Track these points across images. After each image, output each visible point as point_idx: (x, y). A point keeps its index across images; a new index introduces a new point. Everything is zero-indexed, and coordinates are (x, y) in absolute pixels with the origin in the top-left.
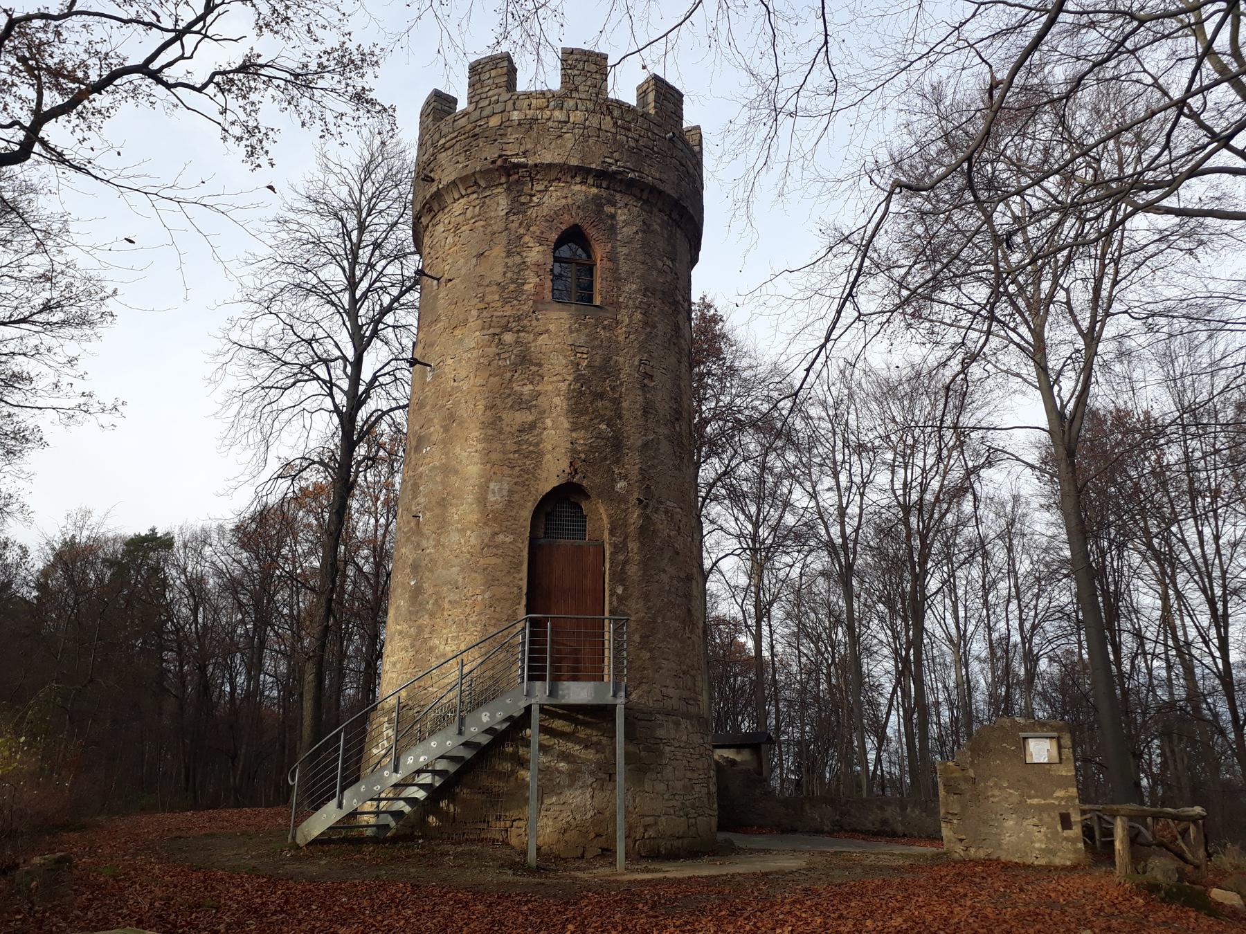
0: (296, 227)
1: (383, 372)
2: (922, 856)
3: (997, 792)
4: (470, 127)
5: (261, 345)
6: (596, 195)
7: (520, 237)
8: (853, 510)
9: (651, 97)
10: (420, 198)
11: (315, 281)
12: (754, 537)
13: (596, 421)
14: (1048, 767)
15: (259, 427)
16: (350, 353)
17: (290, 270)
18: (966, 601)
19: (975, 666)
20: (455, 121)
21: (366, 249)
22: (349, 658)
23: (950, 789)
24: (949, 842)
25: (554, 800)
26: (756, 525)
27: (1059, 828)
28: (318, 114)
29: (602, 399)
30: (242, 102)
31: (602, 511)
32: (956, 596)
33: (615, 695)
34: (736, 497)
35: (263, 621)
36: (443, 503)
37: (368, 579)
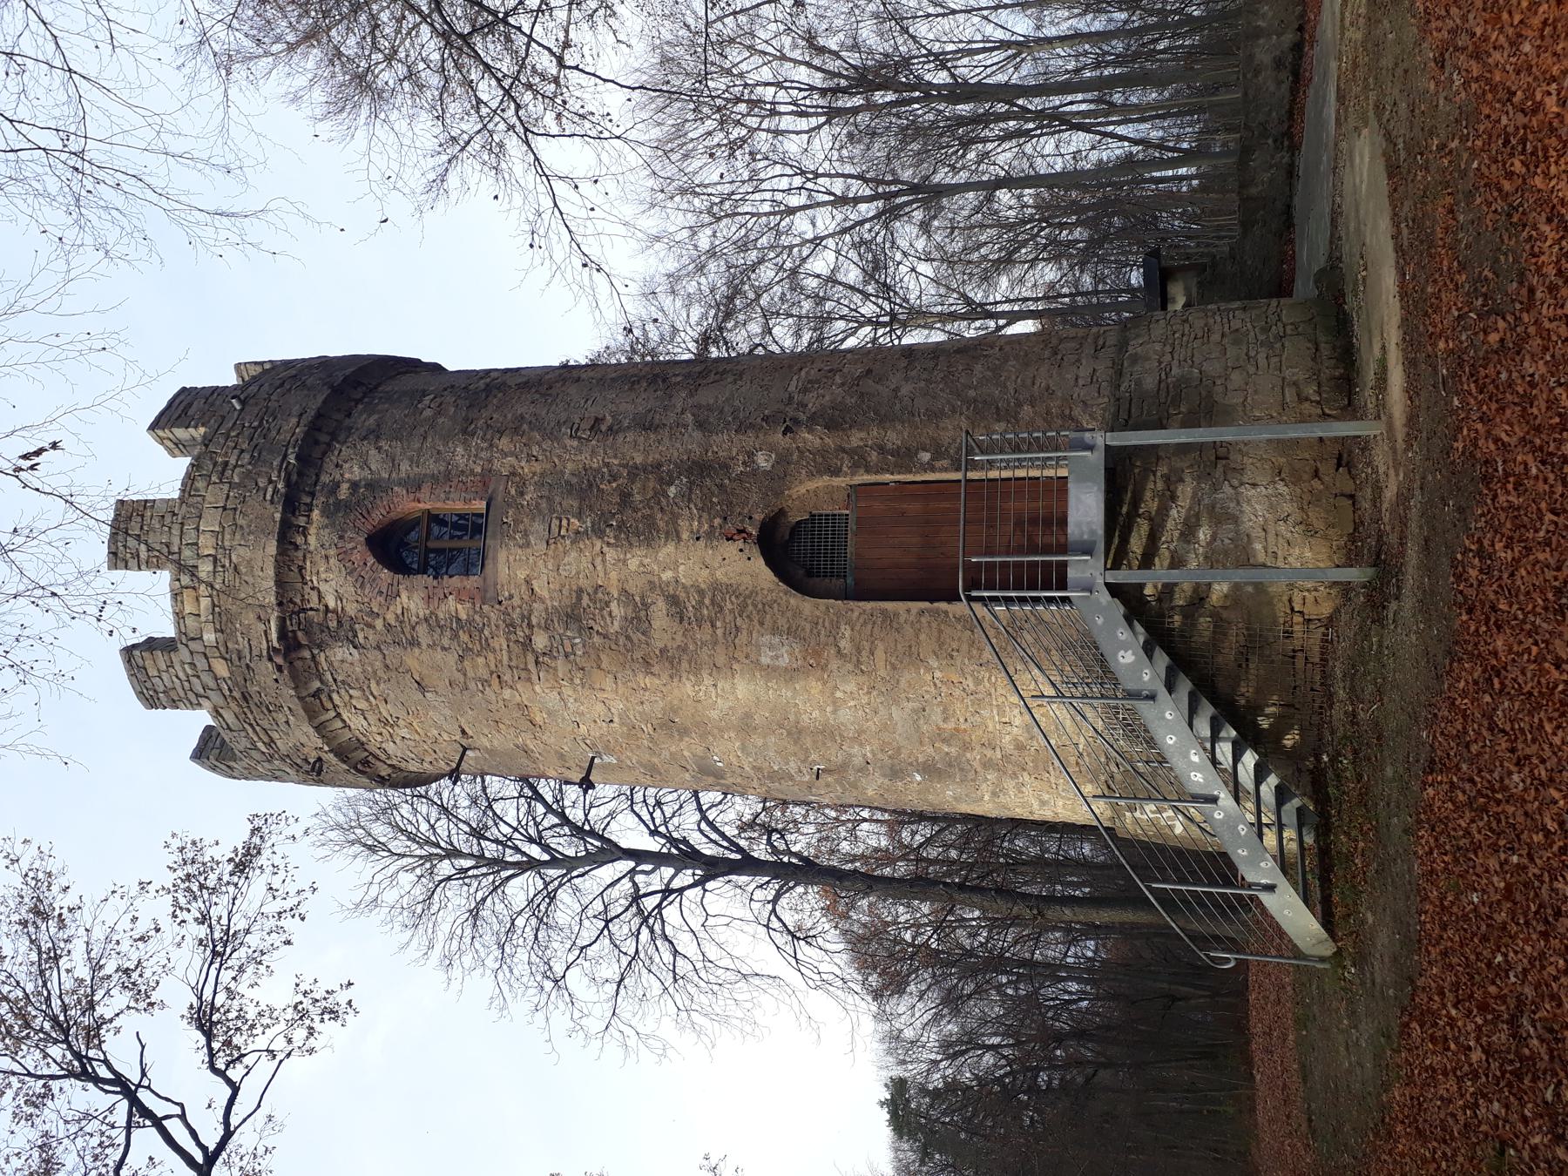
0: (455, 943)
4: (233, 705)
6: (324, 513)
7: (388, 626)
8: (838, 187)
9: (181, 433)
10: (350, 778)
13: (664, 502)
18: (961, 41)
20: (229, 728)
25: (1258, 546)
29: (630, 495)
33: (1091, 448)
35: (997, 962)
36: (797, 733)
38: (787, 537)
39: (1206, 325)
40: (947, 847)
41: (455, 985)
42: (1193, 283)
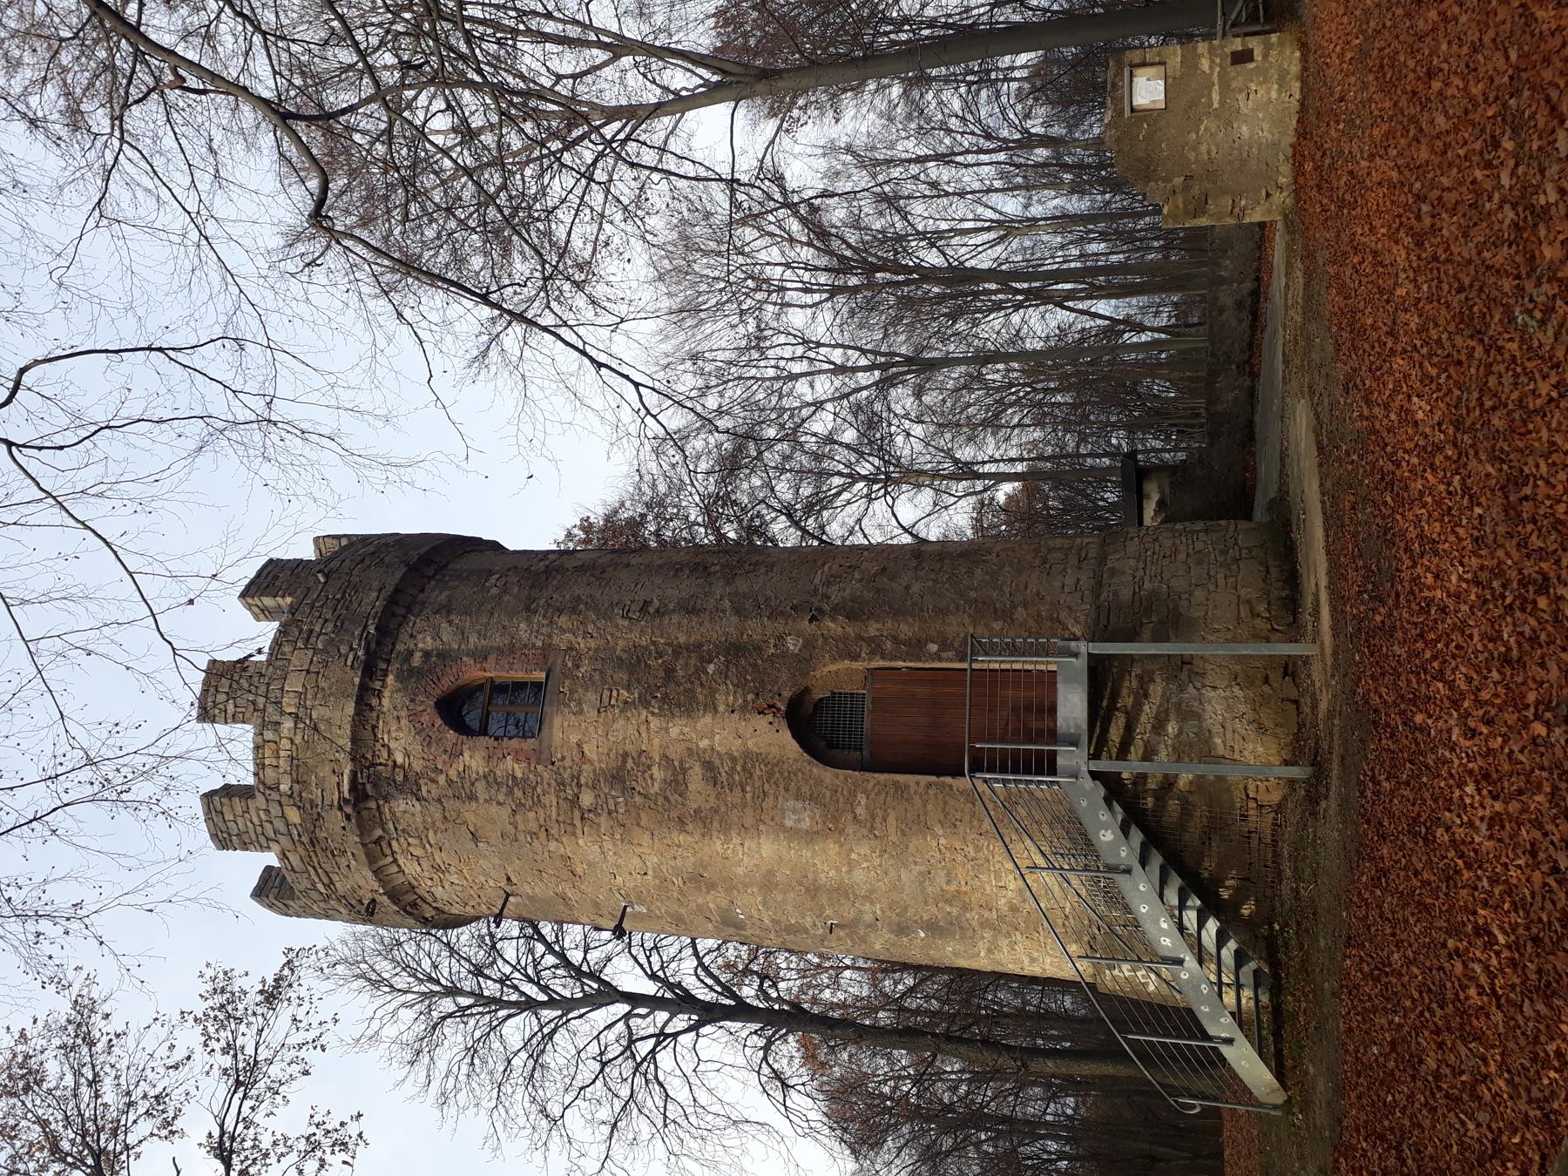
0: (451, 1080)
1: (646, 966)
2: (1289, 249)
3: (1204, 148)
4: (300, 849)
5: (606, 1130)
6: (398, 678)
7: (450, 782)
8: (837, 356)
9: (268, 601)
10: (398, 918)
11: (523, 1055)
12: (870, 480)
13: (703, 677)
14: (1170, 80)
15: (718, 1132)
16: (622, 1008)
17: (507, 1089)
18: (954, 219)
19: (1036, 210)
20: (293, 870)
21: (483, 986)
22: (1025, 1003)
23: (1200, 210)
24: (1269, 212)
25: (1218, 741)
26: (854, 478)
27: (1251, 66)
28: (293, 1053)
29: (674, 670)
30: (272, 1159)
31: (826, 670)
32: (950, 230)
33: (1076, 655)
34: (817, 504)
35: (976, 1118)
36: (813, 890)
37: (922, 981)
38: (811, 712)
39: (1174, 544)
40: (927, 998)
41: (451, 1122)
42: (1166, 483)
